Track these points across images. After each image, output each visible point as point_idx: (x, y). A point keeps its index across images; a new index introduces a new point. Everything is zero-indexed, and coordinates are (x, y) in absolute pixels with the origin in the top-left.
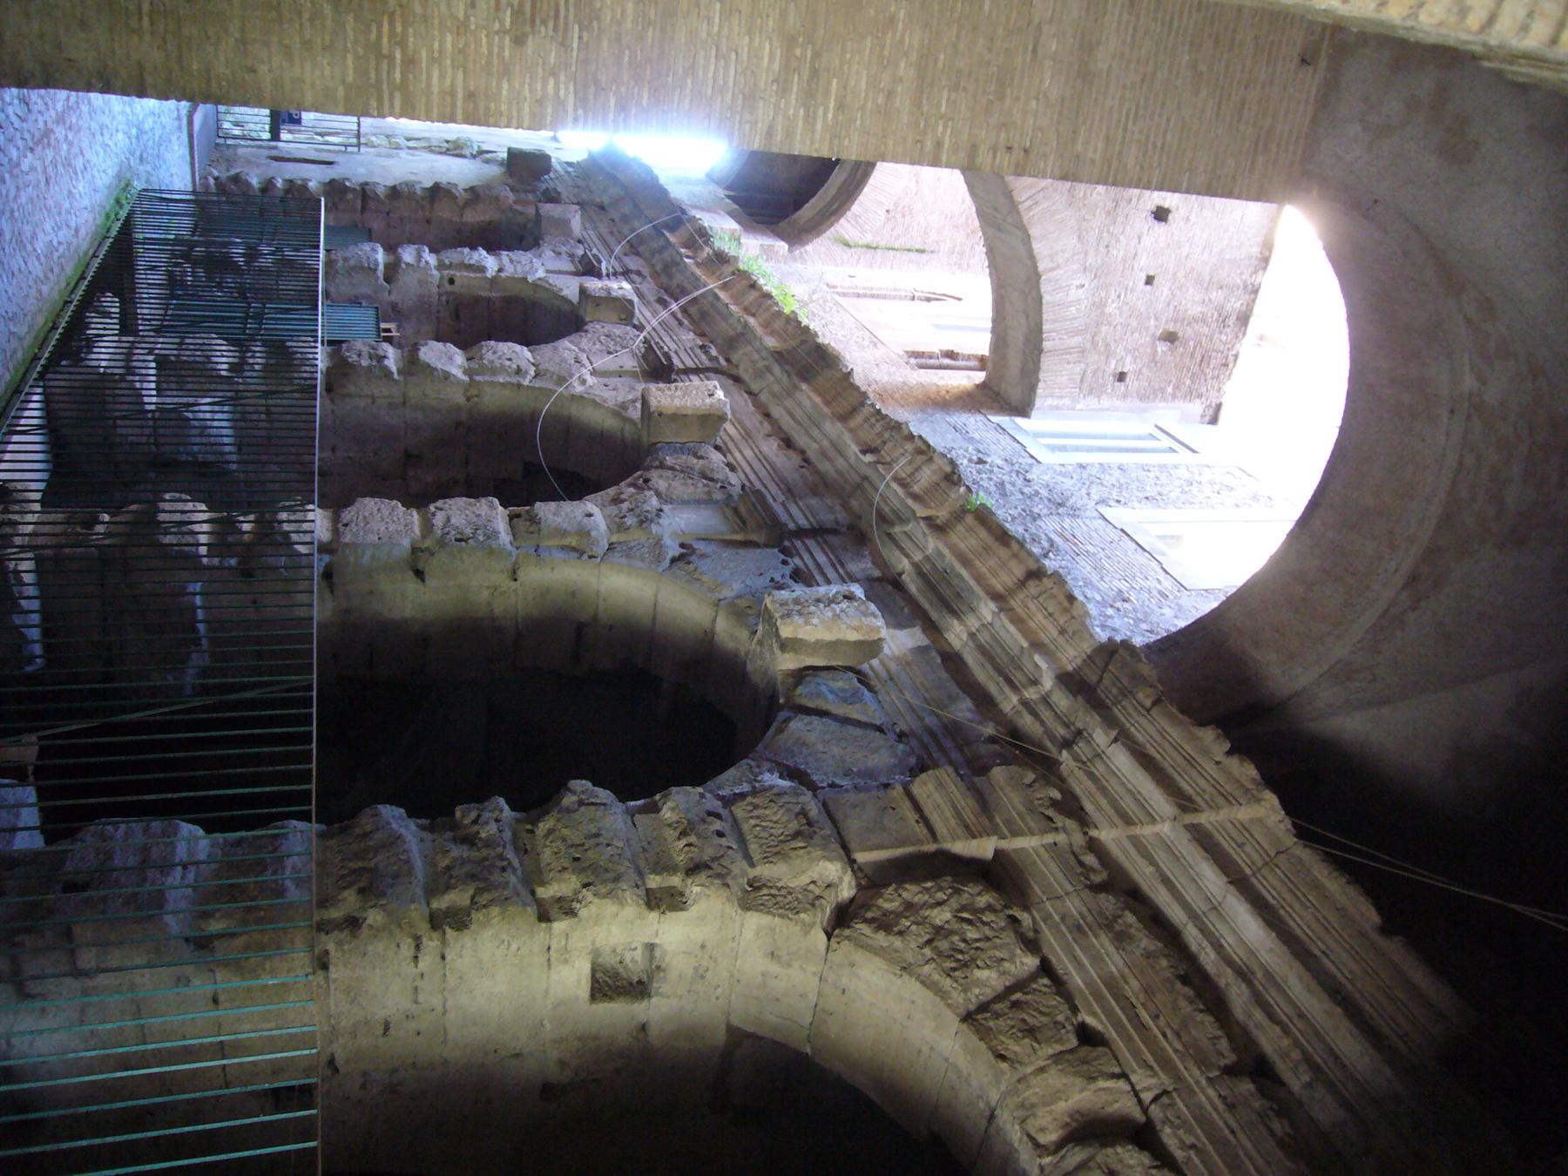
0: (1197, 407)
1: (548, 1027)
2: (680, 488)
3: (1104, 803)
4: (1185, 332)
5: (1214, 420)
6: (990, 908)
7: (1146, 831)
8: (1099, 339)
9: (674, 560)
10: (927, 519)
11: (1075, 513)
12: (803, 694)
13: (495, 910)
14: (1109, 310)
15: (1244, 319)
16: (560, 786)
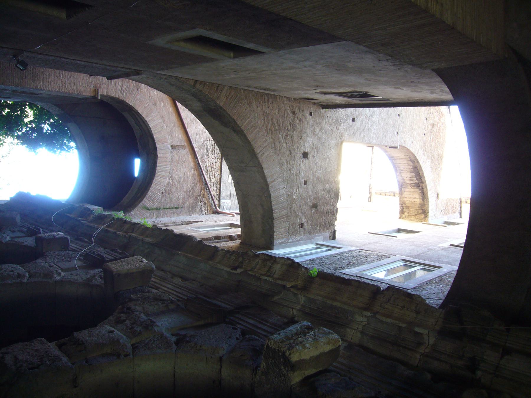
4: (320, 203)
14: (294, 197)
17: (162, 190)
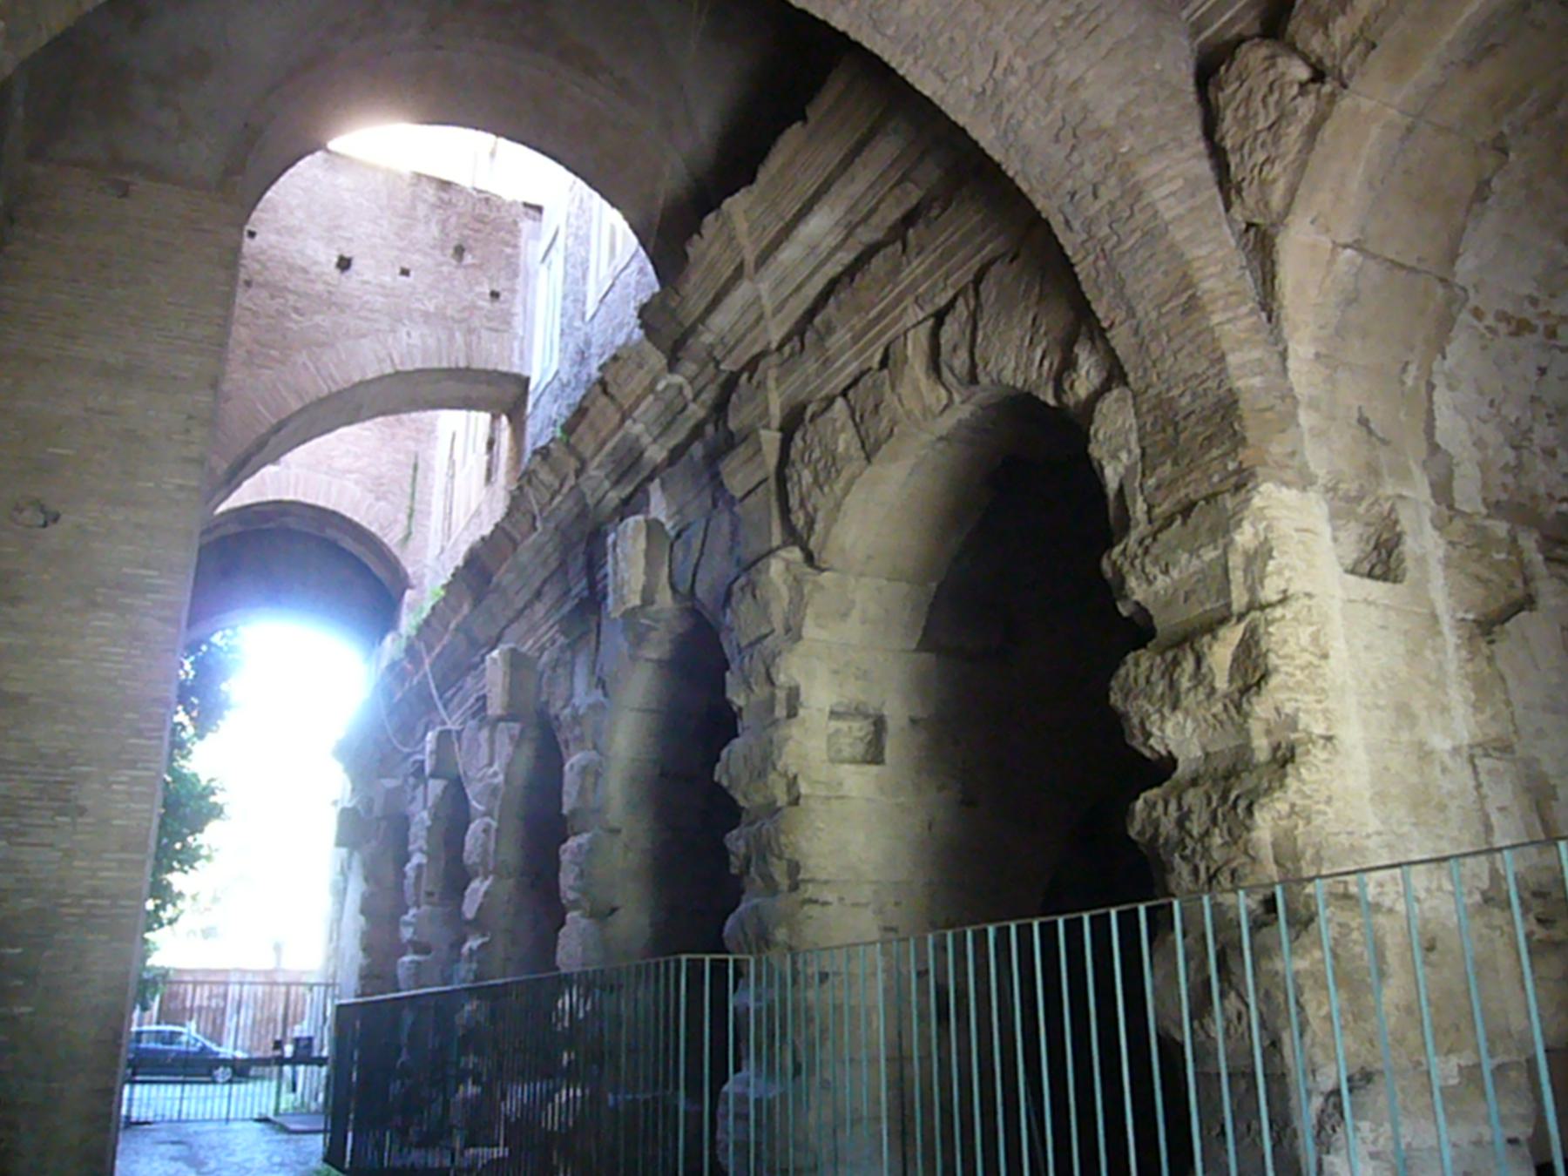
0: (526, 225)
1: (902, 799)
2: (561, 690)
3: (749, 337)
5: (539, 209)
6: (804, 439)
7: (768, 306)
8: (457, 316)
9: (606, 695)
10: (577, 477)
11: (588, 343)
12: (684, 588)
13: (783, 839)
14: (432, 309)
15: (445, 185)
16: (718, 785)
17: (370, 498)
